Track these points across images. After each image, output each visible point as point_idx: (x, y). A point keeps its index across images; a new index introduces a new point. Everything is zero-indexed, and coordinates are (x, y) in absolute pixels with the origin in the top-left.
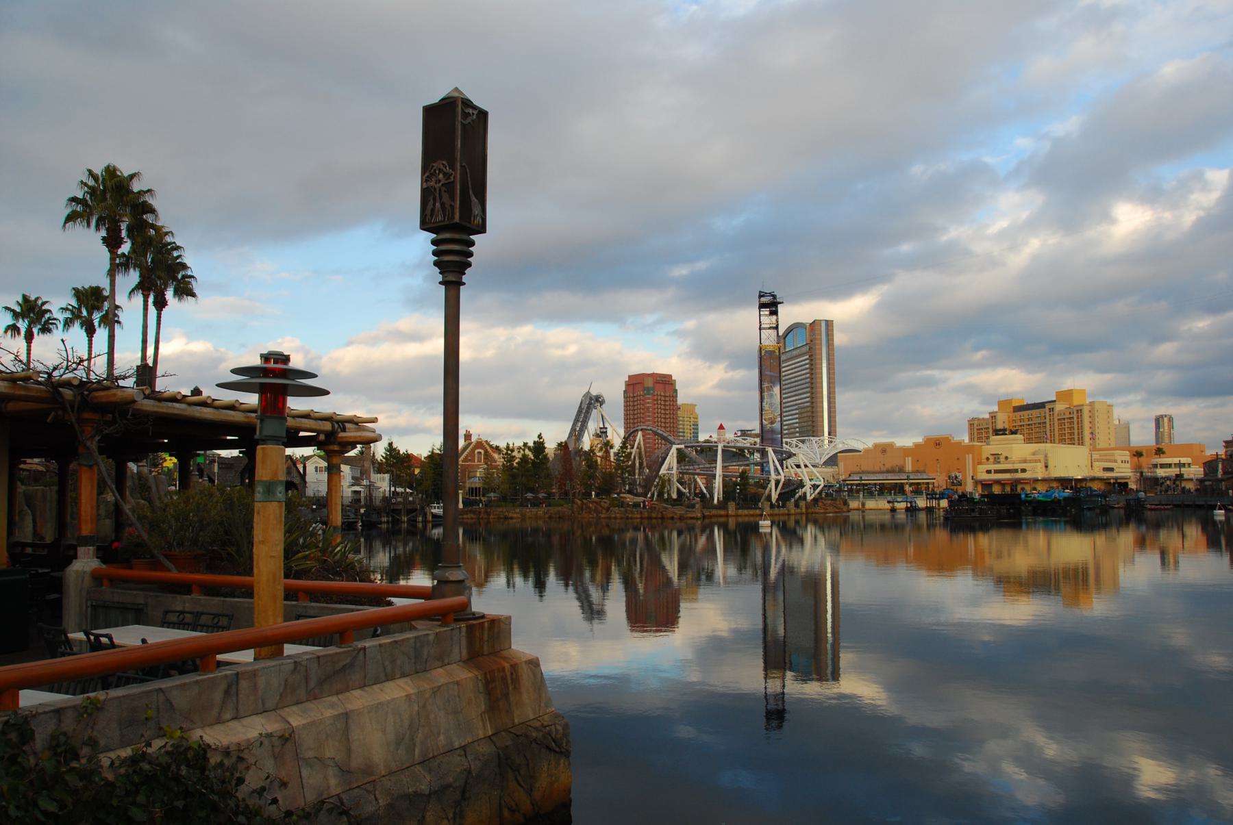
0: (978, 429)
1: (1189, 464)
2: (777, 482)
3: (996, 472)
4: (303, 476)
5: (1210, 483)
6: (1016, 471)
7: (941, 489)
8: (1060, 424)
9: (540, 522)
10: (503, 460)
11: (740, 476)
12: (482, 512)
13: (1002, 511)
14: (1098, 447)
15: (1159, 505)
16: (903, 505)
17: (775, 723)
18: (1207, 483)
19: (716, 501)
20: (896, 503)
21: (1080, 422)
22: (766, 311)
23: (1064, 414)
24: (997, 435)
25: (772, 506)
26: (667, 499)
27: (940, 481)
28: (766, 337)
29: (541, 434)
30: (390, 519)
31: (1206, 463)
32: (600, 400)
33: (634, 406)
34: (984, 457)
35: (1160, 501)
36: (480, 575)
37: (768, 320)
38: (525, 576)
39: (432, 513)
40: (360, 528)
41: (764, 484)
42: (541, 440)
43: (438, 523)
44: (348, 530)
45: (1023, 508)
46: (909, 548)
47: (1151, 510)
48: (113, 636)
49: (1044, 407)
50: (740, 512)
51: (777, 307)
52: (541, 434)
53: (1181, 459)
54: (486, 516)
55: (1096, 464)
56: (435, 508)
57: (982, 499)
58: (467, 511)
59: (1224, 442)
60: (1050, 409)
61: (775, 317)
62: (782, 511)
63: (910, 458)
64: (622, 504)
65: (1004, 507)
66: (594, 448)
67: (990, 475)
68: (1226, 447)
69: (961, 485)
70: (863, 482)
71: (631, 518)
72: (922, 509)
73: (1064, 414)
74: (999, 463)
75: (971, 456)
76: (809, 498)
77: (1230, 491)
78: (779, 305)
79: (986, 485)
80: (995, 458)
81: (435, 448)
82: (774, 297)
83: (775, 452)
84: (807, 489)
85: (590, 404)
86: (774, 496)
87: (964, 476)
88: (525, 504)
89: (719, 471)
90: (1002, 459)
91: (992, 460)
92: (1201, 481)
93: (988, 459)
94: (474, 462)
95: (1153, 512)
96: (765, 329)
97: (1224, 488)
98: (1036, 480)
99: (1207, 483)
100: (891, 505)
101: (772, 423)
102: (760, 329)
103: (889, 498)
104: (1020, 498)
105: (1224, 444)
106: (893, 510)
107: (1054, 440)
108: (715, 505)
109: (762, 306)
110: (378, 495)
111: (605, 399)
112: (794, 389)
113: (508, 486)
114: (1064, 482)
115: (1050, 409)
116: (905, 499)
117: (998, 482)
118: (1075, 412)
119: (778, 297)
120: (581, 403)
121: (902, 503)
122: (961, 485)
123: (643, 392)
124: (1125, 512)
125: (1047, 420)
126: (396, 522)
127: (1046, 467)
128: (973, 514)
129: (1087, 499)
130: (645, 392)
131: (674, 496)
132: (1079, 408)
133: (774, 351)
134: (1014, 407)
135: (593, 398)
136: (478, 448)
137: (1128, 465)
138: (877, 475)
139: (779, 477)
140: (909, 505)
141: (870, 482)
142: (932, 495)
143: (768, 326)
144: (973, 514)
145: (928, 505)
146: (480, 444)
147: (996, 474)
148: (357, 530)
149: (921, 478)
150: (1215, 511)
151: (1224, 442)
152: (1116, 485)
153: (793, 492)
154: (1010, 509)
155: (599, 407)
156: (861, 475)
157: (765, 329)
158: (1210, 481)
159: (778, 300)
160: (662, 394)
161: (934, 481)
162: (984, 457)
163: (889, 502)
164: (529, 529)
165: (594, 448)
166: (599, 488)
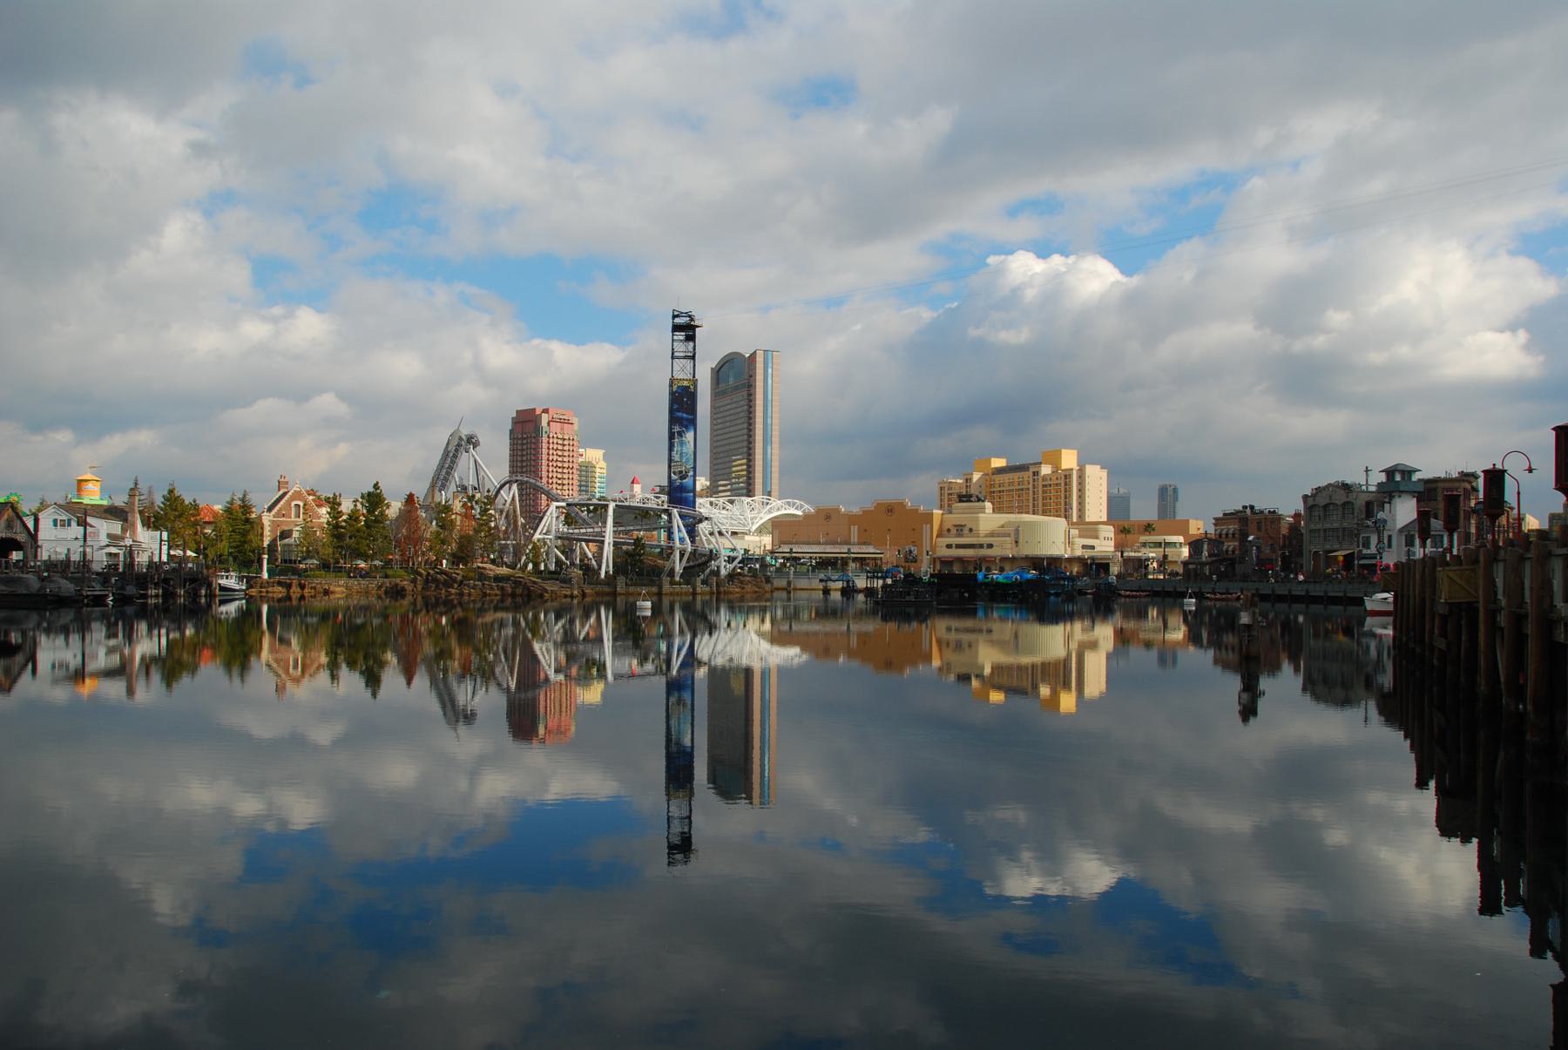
0: (949, 494)
1: (1181, 543)
3: (959, 546)
4: (34, 537)
6: (981, 546)
7: (889, 566)
9: (373, 600)
10: (328, 516)
11: (634, 544)
12: (294, 585)
16: (839, 585)
17: (679, 857)
18: (1191, 566)
19: (603, 575)
21: (1068, 490)
22: (681, 336)
23: (1051, 479)
24: (960, 501)
25: (672, 583)
29: (377, 483)
30: (161, 591)
31: (1192, 542)
32: (474, 441)
33: (523, 450)
34: (946, 528)
35: (1140, 587)
37: (681, 348)
38: (352, 665)
39: (220, 584)
40: (111, 603)
41: (667, 553)
42: (379, 491)
43: (231, 597)
44: (93, 606)
45: (978, 592)
47: (1126, 597)
48: (1409, 749)
49: (1028, 470)
50: (631, 589)
51: (694, 332)
52: (377, 483)
54: (299, 590)
58: (274, 583)
59: (1214, 519)
60: (1034, 473)
61: (691, 344)
64: (482, 576)
66: (450, 503)
68: (1215, 525)
69: (916, 561)
70: (794, 555)
71: (490, 595)
72: (860, 591)
73: (1051, 479)
76: (723, 572)
77: (1214, 576)
78: (697, 329)
80: (957, 530)
81: (235, 498)
82: (692, 318)
83: (682, 516)
85: (459, 445)
86: (678, 569)
88: (374, 574)
89: (609, 539)
90: (966, 531)
91: (954, 531)
94: (291, 518)
96: (678, 358)
97: (1207, 574)
99: (1191, 566)
100: (824, 584)
101: (682, 478)
102: (673, 358)
103: (822, 576)
105: (1214, 521)
108: (602, 580)
110: (142, 559)
111: (480, 440)
113: (331, 550)
115: (1034, 473)
117: (960, 560)
118: (1063, 478)
119: (696, 318)
120: (448, 444)
121: (837, 583)
122: (916, 561)
125: (1031, 486)
126: (169, 595)
127: (1016, 542)
128: (908, 598)
129: (1053, 582)
131: (552, 567)
132: (1067, 473)
133: (689, 387)
134: (1188, 521)
135: (464, 438)
136: (293, 500)
138: (813, 546)
140: (845, 585)
141: (804, 555)
143: (682, 354)
144: (908, 598)
145: (869, 586)
147: (958, 550)
148: (107, 605)
149: (867, 551)
150: (1185, 600)
151: (1214, 519)
152: (1094, 567)
153: (705, 564)
154: (964, 592)
156: (790, 546)
157: (678, 358)
159: (696, 323)
160: (560, 436)
161: (882, 556)
163: (821, 581)
165: (450, 503)
166: (454, 555)
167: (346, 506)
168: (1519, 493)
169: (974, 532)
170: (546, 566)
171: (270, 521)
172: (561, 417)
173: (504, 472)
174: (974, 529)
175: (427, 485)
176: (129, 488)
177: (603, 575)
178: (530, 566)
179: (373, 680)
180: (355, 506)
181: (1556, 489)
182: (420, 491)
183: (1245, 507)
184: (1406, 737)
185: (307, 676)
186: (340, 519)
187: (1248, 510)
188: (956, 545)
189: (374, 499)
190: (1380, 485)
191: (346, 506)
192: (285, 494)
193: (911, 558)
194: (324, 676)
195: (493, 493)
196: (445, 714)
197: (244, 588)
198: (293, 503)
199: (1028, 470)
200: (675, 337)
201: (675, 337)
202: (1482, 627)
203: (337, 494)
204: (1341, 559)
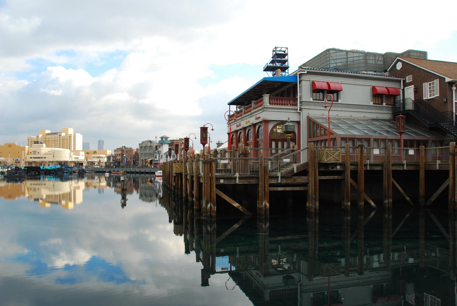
3: (34, 158)
5: (108, 164)
6: (42, 158)
8: (63, 141)
15: (117, 171)
18: (107, 164)
24: (35, 143)
27: (10, 161)
35: (92, 170)
45: (41, 172)
47: (88, 173)
49: (58, 134)
53: (100, 155)
57: (25, 168)
60: (59, 135)
65: (34, 172)
75: (24, 151)
87: (21, 159)
90: (37, 153)
91: (32, 153)
92: (106, 163)
93: (31, 153)
95: (89, 174)
99: (107, 164)
104: (40, 168)
105: (114, 151)
107: (61, 147)
114: (60, 163)
115: (59, 135)
117: (35, 162)
118: (69, 137)
122: (19, 163)
124: (78, 174)
125: (58, 139)
128: (16, 175)
129: (65, 169)
132: (70, 135)
137: (84, 157)
144: (16, 175)
145: (2, 171)
158: (108, 163)
168: (193, 144)
169: (39, 153)
181: (201, 143)
187: (124, 148)
188: (33, 157)
193: (17, 162)
199: (58, 134)
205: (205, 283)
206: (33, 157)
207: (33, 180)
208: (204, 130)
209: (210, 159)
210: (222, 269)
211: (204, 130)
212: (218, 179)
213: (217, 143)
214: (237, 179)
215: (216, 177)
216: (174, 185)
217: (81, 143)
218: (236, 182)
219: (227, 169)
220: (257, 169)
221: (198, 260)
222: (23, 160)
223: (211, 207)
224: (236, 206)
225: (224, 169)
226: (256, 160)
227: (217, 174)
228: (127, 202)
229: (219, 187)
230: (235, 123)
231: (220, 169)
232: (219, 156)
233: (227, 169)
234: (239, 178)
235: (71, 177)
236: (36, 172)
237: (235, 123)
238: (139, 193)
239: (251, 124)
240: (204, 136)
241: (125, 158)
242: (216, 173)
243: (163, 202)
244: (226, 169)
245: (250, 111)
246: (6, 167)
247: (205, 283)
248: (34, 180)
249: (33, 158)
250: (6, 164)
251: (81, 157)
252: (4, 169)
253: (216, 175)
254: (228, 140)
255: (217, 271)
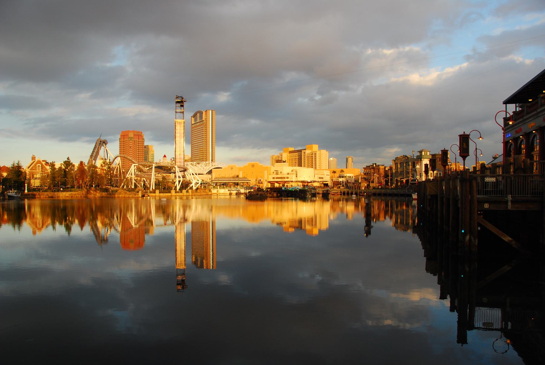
2: (179, 181)
6: (284, 178)
13: (275, 195)
14: (322, 169)
20: (231, 191)
22: (179, 105)
24: (277, 162)
25: (176, 192)
26: (61, 188)
28: (178, 116)
29: (69, 157)
36: (39, 224)
38: (61, 223)
39: (8, 195)
42: (69, 160)
45: (283, 194)
46: (240, 210)
52: (69, 157)
55: (316, 176)
56: (10, 192)
62: (181, 194)
63: (241, 172)
67: (274, 179)
69: (262, 183)
74: (278, 174)
75: (266, 171)
76: (194, 188)
79: (272, 183)
81: (15, 163)
82: (182, 98)
84: (193, 184)
86: (178, 188)
90: (279, 173)
93: (273, 173)
98: (292, 182)
100: (230, 191)
106: (230, 194)
109: (178, 102)
112: (197, 140)
116: (235, 189)
117: (277, 182)
122: (262, 183)
123: (128, 139)
127: (297, 176)
130: (129, 139)
136: (37, 164)
137: (329, 177)
139: (180, 179)
140: (237, 192)
142: (247, 188)
144: (257, 196)
145: (245, 192)
146: (39, 162)
149: (245, 180)
155: (105, 146)
162: (272, 172)
163: (229, 190)
164: (309, 201)
167: (57, 166)
168: (456, 158)
170: (131, 187)
171: (28, 172)
172: (138, 134)
173: (117, 153)
174: (282, 172)
175: (89, 158)
176: (401, 155)
177: (151, 189)
178: (125, 187)
179: (68, 228)
180: (61, 166)
181: (460, 156)
182: (86, 162)
183: (373, 164)
184: (420, 241)
185: (45, 227)
186: (55, 171)
187: (374, 165)
188: (276, 177)
189: (68, 163)
190: (417, 156)
191: (57, 166)
192: (34, 162)
193: (260, 182)
194: (51, 227)
195: (111, 161)
196: (97, 240)
197: (19, 196)
198: (37, 165)
200: (177, 105)
201: (177, 105)
202: (439, 202)
203: (54, 161)
204: (404, 181)
205: (462, 339)
206: (275, 178)
207: (252, 201)
208: (464, 139)
209: (470, 176)
210: (484, 324)
211: (464, 139)
212: (481, 202)
213: (494, 156)
214: (510, 204)
215: (477, 200)
216: (429, 210)
217: (326, 161)
218: (507, 207)
219: (499, 190)
220: (535, 189)
221: (452, 309)
222: (266, 180)
223: (470, 239)
224: (507, 241)
225: (495, 190)
226: (531, 177)
227: (478, 196)
228: (372, 230)
229: (486, 214)
230: (513, 128)
231: (488, 191)
232: (488, 173)
233: (499, 190)
234: (512, 202)
235: (314, 198)
236: (278, 194)
237: (513, 128)
238: (32, 214)
239: (537, 127)
240: (465, 146)
241: (376, 178)
242: (479, 195)
243: (416, 229)
244: (497, 191)
245: (536, 110)
246: (249, 188)
247: (462, 339)
248: (253, 202)
249: (276, 179)
250: (250, 185)
251: (327, 179)
252: (247, 190)
253: (477, 198)
254: (502, 153)
255: (476, 326)
